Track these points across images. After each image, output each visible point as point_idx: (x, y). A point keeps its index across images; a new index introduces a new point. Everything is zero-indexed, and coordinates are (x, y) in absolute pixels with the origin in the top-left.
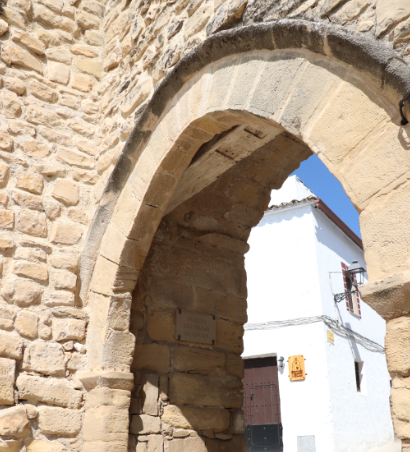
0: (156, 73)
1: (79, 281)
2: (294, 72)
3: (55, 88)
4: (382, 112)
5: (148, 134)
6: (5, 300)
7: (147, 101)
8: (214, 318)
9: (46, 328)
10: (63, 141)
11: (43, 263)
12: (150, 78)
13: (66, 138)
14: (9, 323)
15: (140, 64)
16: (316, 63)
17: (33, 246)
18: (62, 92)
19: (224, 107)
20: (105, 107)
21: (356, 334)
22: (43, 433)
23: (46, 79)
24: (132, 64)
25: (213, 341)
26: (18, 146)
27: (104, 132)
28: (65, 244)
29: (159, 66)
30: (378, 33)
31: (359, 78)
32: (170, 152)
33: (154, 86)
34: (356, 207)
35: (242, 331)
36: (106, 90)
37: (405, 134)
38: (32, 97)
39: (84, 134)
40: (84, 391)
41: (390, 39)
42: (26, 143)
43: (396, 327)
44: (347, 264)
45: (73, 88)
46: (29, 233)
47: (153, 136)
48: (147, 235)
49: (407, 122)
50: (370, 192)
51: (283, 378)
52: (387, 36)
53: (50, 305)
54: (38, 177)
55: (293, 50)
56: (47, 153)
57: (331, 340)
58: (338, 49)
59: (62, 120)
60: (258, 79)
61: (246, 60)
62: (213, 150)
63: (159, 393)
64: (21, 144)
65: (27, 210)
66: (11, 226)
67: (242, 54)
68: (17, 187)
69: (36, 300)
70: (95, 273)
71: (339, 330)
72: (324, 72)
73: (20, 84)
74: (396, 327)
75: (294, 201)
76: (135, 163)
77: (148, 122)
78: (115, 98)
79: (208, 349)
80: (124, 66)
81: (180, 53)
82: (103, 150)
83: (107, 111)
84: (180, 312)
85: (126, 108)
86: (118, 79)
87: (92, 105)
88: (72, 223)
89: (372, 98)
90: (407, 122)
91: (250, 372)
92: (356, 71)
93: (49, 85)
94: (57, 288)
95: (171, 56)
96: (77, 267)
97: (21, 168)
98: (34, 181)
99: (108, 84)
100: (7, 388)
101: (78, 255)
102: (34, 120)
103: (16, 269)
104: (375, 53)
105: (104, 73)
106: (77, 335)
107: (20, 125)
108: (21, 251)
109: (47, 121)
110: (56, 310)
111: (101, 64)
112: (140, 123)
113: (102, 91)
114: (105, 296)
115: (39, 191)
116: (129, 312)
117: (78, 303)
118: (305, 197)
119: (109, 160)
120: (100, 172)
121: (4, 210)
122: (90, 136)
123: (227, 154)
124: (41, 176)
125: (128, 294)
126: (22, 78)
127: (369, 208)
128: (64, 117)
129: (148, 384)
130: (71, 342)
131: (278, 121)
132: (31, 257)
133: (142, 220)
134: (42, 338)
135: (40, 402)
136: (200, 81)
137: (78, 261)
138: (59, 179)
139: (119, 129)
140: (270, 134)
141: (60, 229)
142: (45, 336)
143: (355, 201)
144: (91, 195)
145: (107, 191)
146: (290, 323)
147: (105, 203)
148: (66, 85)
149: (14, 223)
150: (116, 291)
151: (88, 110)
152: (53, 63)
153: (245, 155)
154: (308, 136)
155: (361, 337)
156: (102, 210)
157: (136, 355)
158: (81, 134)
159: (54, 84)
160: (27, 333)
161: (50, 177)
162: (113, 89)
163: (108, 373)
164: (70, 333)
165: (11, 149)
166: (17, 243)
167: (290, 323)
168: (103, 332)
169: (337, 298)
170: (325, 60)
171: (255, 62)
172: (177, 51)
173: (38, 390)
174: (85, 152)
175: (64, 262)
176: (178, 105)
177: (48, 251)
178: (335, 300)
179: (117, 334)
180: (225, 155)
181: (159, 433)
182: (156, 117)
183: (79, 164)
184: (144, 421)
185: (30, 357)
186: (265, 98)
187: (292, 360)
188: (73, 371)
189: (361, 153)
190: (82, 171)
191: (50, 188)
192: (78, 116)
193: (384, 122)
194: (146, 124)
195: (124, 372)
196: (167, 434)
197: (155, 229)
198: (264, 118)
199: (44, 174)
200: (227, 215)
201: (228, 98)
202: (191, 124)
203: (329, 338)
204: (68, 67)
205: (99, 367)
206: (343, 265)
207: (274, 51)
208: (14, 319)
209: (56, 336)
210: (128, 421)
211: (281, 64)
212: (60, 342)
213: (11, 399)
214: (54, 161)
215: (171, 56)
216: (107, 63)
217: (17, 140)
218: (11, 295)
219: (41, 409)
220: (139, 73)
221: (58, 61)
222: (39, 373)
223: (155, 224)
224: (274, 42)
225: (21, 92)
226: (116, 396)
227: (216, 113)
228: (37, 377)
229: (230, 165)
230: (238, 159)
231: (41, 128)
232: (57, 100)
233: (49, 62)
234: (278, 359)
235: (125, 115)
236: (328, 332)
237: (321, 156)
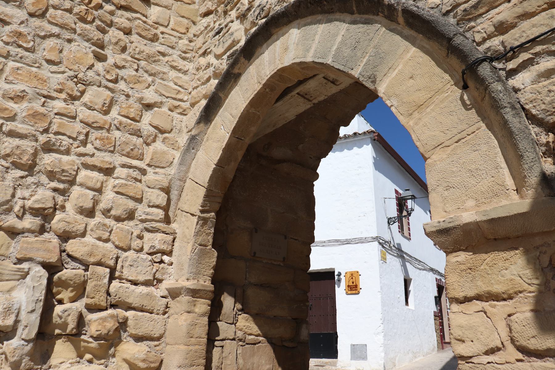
0: (247, 24)
1: (169, 200)
2: (371, 35)
3: (156, 29)
4: (447, 77)
5: (238, 76)
6: (103, 214)
7: (238, 47)
8: (286, 238)
9: (139, 241)
10: (161, 75)
11: (138, 183)
12: (242, 27)
13: (164, 73)
14: (106, 235)
15: (233, 14)
16: (391, 30)
17: (130, 167)
18: (162, 33)
19: (309, 59)
20: (200, 48)
21: (406, 254)
22: (131, 336)
23: (150, 22)
24: (225, 13)
25: (284, 258)
26: (122, 78)
27: (198, 69)
28: (158, 167)
29: (251, 17)
30: (444, 11)
31: (427, 46)
32: (258, 93)
33: (246, 34)
34: (423, 155)
35: (310, 251)
36: (201, 33)
37: (466, 97)
38: (136, 36)
39: (179, 70)
40: (169, 299)
41: (454, 17)
42: (129, 75)
43: (455, 260)
44: (401, 191)
45: (172, 30)
46: (128, 156)
47: (243, 78)
48: (233, 163)
49: (468, 87)
50: (435, 143)
51: (340, 292)
52: (452, 14)
53: (143, 221)
54: (138, 106)
55: (371, 17)
56: (147, 85)
57: (384, 259)
58: (411, 20)
59: (161, 58)
60: (339, 39)
61: (329, 21)
62: (294, 93)
63: (235, 303)
64: (125, 77)
65: (127, 135)
66: (112, 149)
67: (326, 15)
68: (119, 114)
69: (131, 216)
70: (184, 194)
71: (391, 250)
72: (398, 38)
73: (127, 24)
74: (455, 260)
75: (355, 134)
76: (225, 100)
77: (239, 65)
78: (210, 41)
79: (279, 265)
80: (219, 14)
81: (270, 8)
82: (196, 85)
83: (201, 52)
84: (256, 232)
85: (219, 51)
86: (212, 25)
87: (188, 45)
88: (166, 149)
89: (439, 64)
90: (468, 87)
91: (313, 284)
92: (426, 41)
93: (152, 26)
94: (149, 206)
95: (262, 10)
96: (168, 187)
97: (123, 98)
98: (134, 109)
99: (203, 29)
100: (101, 294)
101: (170, 177)
102: (136, 56)
103: (114, 187)
104: (443, 29)
105: (199, 18)
106: (165, 248)
107: (125, 60)
108: (120, 172)
109: (149, 58)
110: (148, 225)
111: (198, 10)
112: (232, 66)
113: (198, 33)
114: (193, 215)
115: (138, 119)
116: (212, 230)
117: (167, 220)
118: (366, 130)
119: (201, 95)
120: (193, 105)
121: (107, 134)
122: (185, 72)
123: (306, 96)
124: (141, 106)
125: (213, 214)
126: (128, 19)
127: (435, 157)
128: (163, 54)
129: (225, 294)
130: (160, 255)
131: (356, 76)
132: (129, 177)
133: (229, 150)
134: (134, 250)
135: (129, 307)
136: (287, 35)
137: (169, 183)
138: (156, 109)
139: (212, 69)
140: (345, 83)
141: (155, 153)
142: (137, 248)
143: (422, 150)
144: (183, 125)
145: (198, 122)
146: (348, 242)
147: (196, 133)
148: (166, 27)
149: (115, 146)
150: (202, 212)
151: (184, 49)
152: (156, 7)
153: (322, 98)
154: (383, 91)
155: (410, 257)
156: (193, 139)
157: (216, 268)
158: (177, 70)
159: (156, 26)
160: (121, 245)
161: (149, 107)
162: (207, 33)
163: (191, 284)
164: (159, 246)
165: (115, 81)
166: (117, 164)
167: (348, 242)
168: (190, 247)
169: (390, 221)
170: (399, 29)
171: (337, 23)
172: (268, 6)
173: (128, 297)
174: (180, 86)
175: (157, 183)
176: (267, 53)
177: (143, 172)
178: (389, 223)
179: (201, 249)
180: (305, 98)
181: (234, 339)
182: (247, 61)
183: (174, 96)
184: (220, 328)
185: (122, 266)
186: (346, 55)
187: (349, 275)
188: (160, 281)
189: (428, 110)
190: (177, 103)
191: (147, 117)
192: (175, 54)
193: (449, 86)
194: (237, 67)
195: (206, 283)
196: (240, 340)
197: (240, 158)
198: (344, 72)
199: (143, 104)
200: (300, 147)
201: (312, 51)
202: (278, 70)
203: (382, 257)
204: (169, 11)
205: (184, 278)
206: (396, 192)
207: (354, 16)
208: (110, 232)
209: (146, 249)
210: (207, 328)
211: (361, 28)
212: (150, 254)
213: (103, 304)
214: (152, 93)
215: (262, 10)
216: (203, 10)
217: (122, 73)
218: (109, 211)
219: (130, 314)
220: (232, 22)
221: (161, 6)
222: (130, 281)
223: (240, 154)
224: (355, 9)
225: (128, 32)
226: (198, 306)
227: (301, 63)
228: (128, 285)
229: (308, 106)
230: (315, 101)
231: (143, 63)
232: (158, 39)
233: (152, 6)
234: (336, 273)
235: (218, 57)
236: (381, 251)
237: (393, 109)
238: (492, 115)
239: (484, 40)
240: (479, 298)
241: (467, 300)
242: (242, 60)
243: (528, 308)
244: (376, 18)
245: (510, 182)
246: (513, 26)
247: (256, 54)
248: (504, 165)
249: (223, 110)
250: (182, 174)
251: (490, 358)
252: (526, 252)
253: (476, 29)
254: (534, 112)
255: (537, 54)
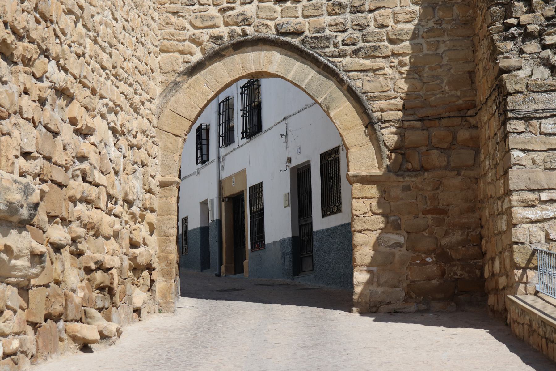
4: (361, 121)
16: (339, 88)
37: (366, 131)
55: (329, 76)
60: (310, 77)
72: (342, 94)
89: (358, 114)
147: (180, 80)
189: (352, 131)
238: (375, 142)
239: (375, 112)
240: (362, 198)
241: (359, 198)
242: (231, 49)
243: (376, 202)
244: (332, 78)
245: (377, 165)
246: (385, 111)
247: (242, 49)
248: (376, 159)
249: (206, 72)
250: (162, 105)
251: (364, 215)
252: (377, 186)
253: (373, 105)
254: (387, 144)
255: (391, 125)
